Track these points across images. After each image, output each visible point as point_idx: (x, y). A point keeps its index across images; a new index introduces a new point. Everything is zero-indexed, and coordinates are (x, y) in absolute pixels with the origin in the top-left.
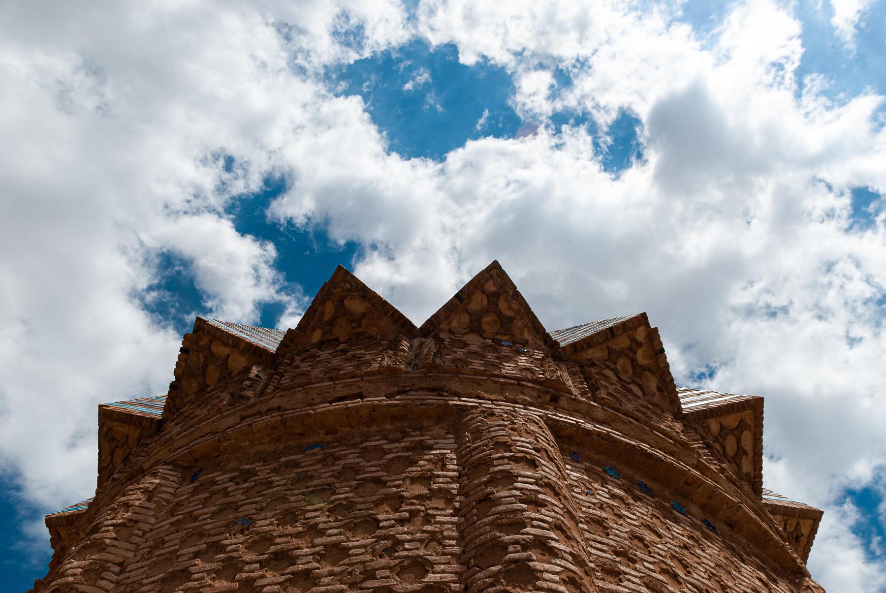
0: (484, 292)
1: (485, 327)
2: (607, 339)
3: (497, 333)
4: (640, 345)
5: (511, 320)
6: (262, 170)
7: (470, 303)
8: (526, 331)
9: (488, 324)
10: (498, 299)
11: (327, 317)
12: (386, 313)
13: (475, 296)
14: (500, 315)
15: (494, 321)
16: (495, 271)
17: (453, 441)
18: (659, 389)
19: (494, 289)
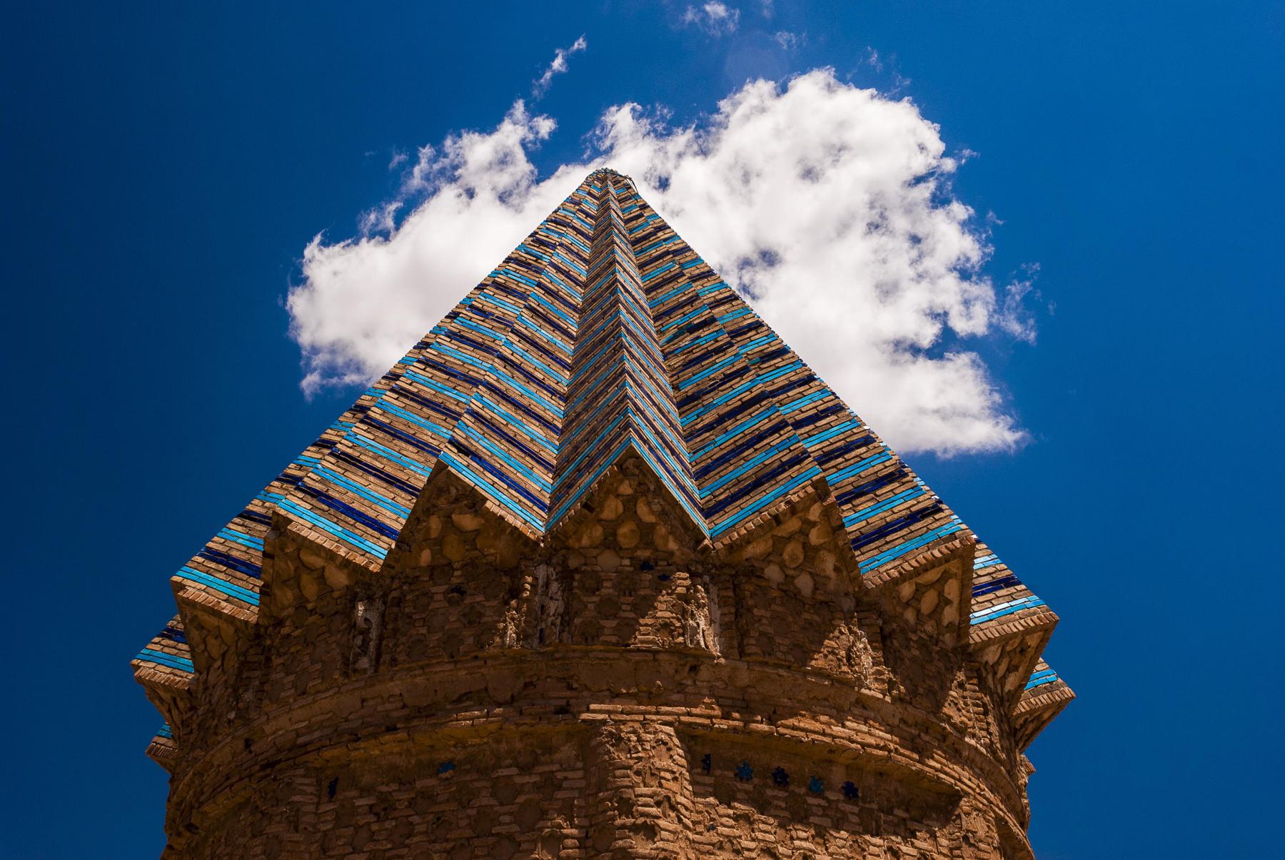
0: (618, 496)
1: (621, 540)
2: (771, 529)
3: (636, 548)
4: (814, 524)
5: (652, 526)
6: (306, 293)
7: (602, 511)
8: (671, 538)
9: (625, 536)
10: (635, 505)
11: (434, 535)
12: (503, 531)
13: (608, 503)
14: (640, 523)
15: (632, 531)
16: (631, 461)
17: (554, 409)
18: (836, 569)
19: (629, 491)
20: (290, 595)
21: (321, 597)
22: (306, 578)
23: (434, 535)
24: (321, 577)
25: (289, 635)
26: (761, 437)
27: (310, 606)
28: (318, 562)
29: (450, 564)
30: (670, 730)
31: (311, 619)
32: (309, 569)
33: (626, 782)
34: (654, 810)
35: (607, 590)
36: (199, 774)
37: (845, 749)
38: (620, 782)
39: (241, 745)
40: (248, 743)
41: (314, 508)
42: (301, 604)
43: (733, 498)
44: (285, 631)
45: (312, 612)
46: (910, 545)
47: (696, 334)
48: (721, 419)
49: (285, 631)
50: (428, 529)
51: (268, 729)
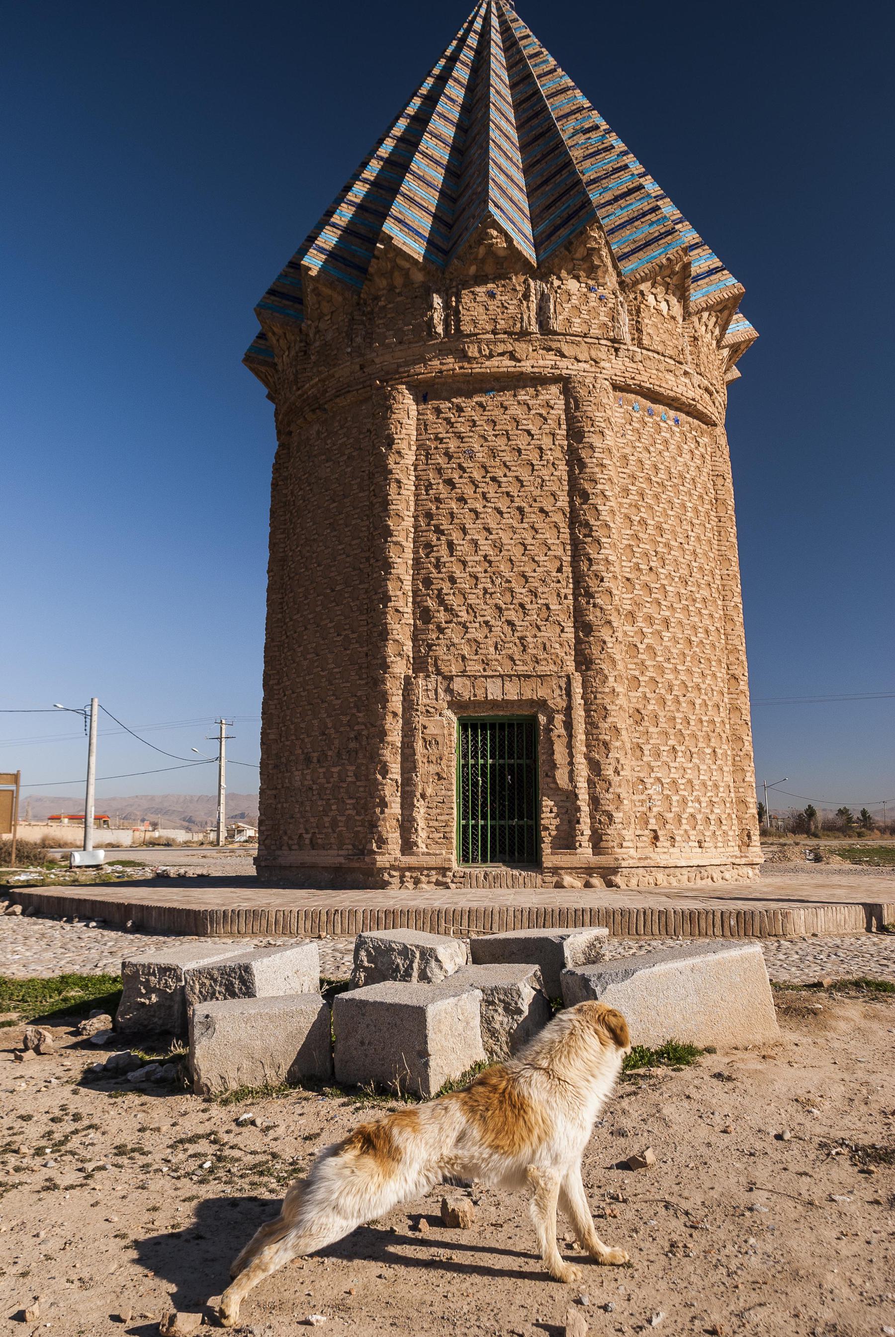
11: (480, 256)
20: (385, 282)
21: (405, 285)
22: (396, 274)
23: (480, 256)
24: (406, 274)
25: (384, 307)
26: (644, 215)
27: (397, 291)
28: (407, 265)
29: (486, 276)
30: (607, 383)
31: (399, 299)
32: (401, 269)
33: (589, 408)
34: (603, 425)
35: (574, 301)
36: (322, 381)
37: (679, 399)
38: (585, 408)
39: (358, 367)
40: (362, 367)
41: (401, 230)
42: (392, 288)
43: (633, 252)
44: (381, 304)
45: (400, 294)
46: (711, 288)
47: (588, 135)
48: (616, 199)
49: (381, 304)
50: (477, 253)
51: (377, 360)
